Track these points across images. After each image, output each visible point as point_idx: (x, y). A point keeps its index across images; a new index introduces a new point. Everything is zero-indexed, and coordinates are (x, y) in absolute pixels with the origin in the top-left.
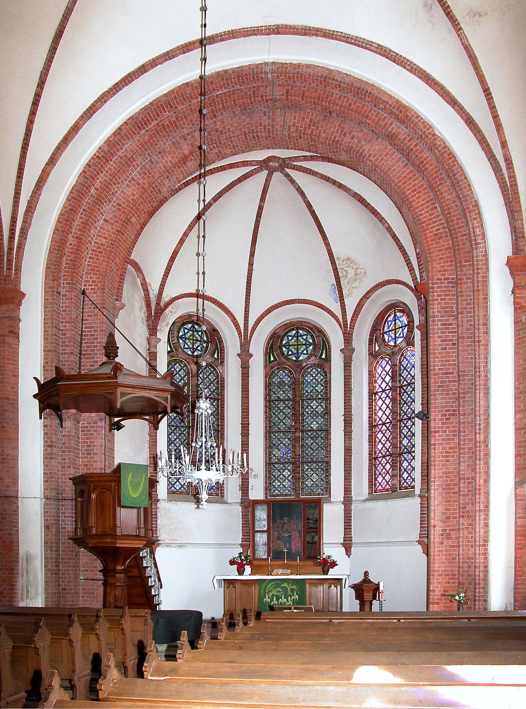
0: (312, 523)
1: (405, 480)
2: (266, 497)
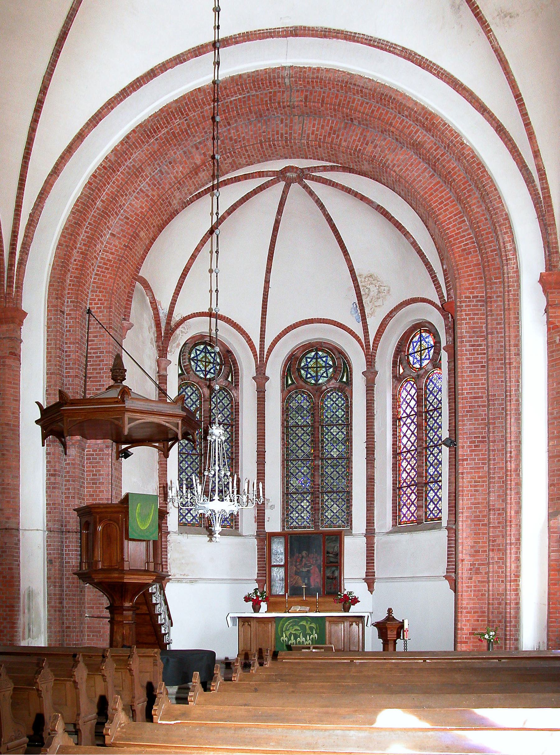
0: (332, 557)
1: (431, 512)
2: (283, 529)
